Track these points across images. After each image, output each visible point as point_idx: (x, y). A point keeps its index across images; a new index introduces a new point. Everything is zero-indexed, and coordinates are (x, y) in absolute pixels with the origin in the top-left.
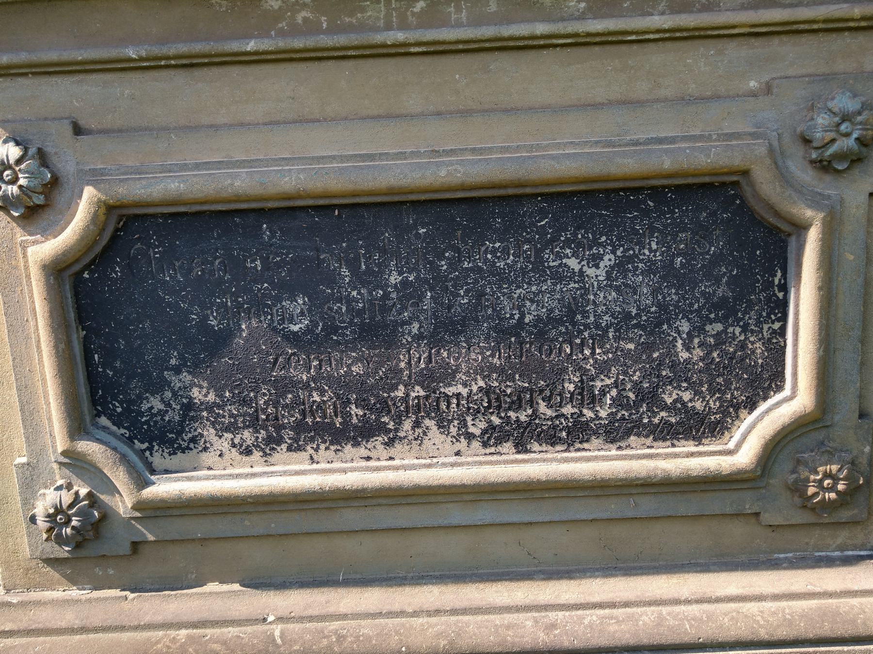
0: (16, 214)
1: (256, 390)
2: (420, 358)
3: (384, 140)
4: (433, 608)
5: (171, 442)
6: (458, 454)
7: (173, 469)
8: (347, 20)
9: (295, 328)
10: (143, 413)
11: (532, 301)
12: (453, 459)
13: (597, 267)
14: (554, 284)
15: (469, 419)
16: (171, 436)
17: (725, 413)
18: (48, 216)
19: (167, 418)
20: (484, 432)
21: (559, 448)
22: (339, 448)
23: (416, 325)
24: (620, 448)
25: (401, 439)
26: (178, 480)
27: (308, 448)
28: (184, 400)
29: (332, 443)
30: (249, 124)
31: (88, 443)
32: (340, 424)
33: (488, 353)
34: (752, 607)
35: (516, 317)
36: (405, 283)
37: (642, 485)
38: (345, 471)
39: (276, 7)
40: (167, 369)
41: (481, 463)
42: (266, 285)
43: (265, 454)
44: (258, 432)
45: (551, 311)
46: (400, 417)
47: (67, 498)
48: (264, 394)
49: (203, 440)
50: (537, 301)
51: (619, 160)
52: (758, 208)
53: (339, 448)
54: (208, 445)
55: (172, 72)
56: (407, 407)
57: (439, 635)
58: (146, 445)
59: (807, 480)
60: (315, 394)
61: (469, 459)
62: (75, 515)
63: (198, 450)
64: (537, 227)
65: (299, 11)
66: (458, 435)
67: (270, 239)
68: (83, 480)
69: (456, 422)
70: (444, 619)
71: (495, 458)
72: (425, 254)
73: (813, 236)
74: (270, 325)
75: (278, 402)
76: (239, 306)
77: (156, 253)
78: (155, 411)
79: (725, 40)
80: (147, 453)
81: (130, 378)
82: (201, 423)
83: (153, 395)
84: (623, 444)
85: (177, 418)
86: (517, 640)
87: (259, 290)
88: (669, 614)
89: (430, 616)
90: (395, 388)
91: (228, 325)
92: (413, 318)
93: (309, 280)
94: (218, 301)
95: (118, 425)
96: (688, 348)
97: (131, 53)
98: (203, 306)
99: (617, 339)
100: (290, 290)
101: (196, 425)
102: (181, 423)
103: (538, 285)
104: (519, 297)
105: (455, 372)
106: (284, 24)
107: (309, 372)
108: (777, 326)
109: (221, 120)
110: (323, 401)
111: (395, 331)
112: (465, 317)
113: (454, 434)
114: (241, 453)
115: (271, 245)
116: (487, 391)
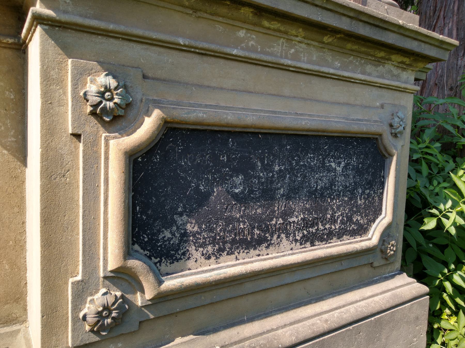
0: (107, 119)
1: (217, 223)
2: (282, 205)
3: (277, 105)
4: (283, 325)
5: (172, 256)
6: (292, 249)
7: (171, 272)
8: (267, 50)
9: (237, 191)
10: (159, 240)
11: (320, 180)
12: (291, 252)
13: (339, 166)
14: (327, 173)
15: (297, 232)
16: (172, 253)
17: (368, 224)
18: (123, 123)
19: (172, 242)
20: (301, 238)
21: (324, 243)
22: (248, 251)
23: (282, 190)
24: (341, 241)
25: (272, 244)
26: (176, 277)
27: (236, 252)
28: (182, 231)
29: (245, 249)
30: (225, 89)
31: (134, 261)
32: (250, 238)
33: (305, 202)
34: (376, 298)
35: (315, 186)
36: (280, 170)
37: (345, 256)
38: (252, 262)
39: (242, 36)
40: (176, 214)
41: (301, 252)
42: (227, 169)
43: (217, 258)
44: (215, 246)
45: (325, 184)
46: (273, 233)
47: (111, 300)
48: (220, 225)
49: (188, 253)
50: (319, 181)
51: (353, 126)
52: (381, 147)
53: (248, 251)
54: (190, 256)
55: (194, 55)
56: (276, 229)
57: (291, 335)
58: (158, 259)
59: (387, 247)
60: (241, 224)
61: (297, 251)
62: (115, 309)
63: (185, 259)
64: (324, 149)
65: (251, 41)
66: (293, 240)
67: (232, 147)
68: (117, 287)
69: (292, 234)
70: (288, 328)
71: (304, 250)
72: (288, 158)
73: (395, 158)
74: (226, 189)
75: (226, 229)
76: (215, 179)
77: (180, 149)
78: (166, 239)
79: (373, 87)
80: (158, 264)
81: (155, 220)
82: (189, 244)
83: (166, 229)
84: (341, 239)
85: (177, 242)
86: (318, 329)
87: (224, 171)
88: (357, 306)
89: (282, 328)
90: (272, 220)
91: (208, 189)
92: (282, 186)
93: (244, 168)
94: (206, 176)
95: (144, 249)
96: (361, 200)
97: (181, 42)
98: (199, 179)
99: (343, 196)
100: (236, 171)
101: (186, 245)
102: (179, 245)
103: (322, 173)
104: (317, 178)
105: (294, 211)
106: (244, 45)
107: (240, 213)
108: (381, 191)
109: (213, 84)
110: (244, 227)
111: (275, 192)
112: (299, 186)
113: (291, 240)
114: (206, 259)
115: (232, 149)
116: (303, 219)
